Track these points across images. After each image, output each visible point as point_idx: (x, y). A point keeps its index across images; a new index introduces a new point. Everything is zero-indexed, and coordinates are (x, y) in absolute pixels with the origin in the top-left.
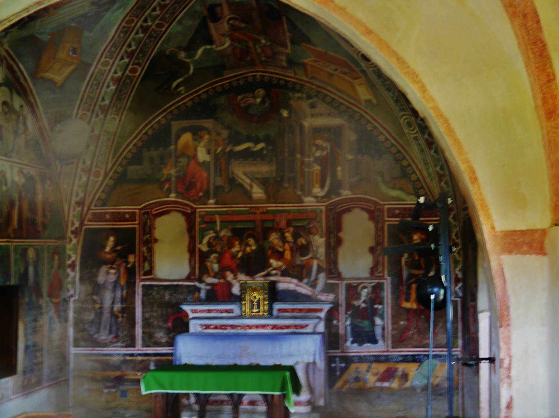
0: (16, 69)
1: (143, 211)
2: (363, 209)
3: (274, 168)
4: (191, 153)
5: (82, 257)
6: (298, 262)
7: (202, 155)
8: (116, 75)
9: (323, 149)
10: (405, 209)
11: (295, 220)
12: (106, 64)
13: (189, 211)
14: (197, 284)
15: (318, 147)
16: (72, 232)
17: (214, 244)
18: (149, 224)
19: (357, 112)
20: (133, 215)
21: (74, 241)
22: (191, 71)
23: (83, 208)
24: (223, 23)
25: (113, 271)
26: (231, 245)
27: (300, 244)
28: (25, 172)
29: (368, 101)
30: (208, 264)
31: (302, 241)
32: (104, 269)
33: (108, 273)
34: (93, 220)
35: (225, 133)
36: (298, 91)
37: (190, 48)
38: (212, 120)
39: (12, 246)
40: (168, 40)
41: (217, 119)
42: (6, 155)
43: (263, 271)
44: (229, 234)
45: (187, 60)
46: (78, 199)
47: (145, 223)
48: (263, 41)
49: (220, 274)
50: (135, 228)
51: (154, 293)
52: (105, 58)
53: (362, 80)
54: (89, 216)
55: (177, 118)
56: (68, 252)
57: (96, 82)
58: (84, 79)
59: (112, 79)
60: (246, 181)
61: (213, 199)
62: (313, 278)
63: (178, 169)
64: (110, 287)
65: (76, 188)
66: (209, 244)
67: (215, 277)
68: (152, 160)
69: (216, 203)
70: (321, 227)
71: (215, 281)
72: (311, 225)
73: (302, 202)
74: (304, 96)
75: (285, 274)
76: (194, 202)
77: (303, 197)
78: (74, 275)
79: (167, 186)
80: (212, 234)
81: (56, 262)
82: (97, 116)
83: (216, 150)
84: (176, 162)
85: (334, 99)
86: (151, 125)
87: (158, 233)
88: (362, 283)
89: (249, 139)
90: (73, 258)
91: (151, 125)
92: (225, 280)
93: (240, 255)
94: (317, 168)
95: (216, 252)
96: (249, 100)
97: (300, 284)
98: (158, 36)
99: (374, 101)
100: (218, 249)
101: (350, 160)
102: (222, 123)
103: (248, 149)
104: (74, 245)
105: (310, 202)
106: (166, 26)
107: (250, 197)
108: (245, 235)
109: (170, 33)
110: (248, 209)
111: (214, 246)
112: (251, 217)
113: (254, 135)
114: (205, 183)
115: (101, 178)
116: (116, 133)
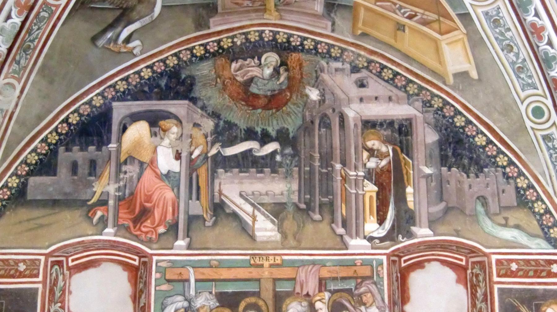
1: (51, 259)
2: (444, 262)
3: (295, 186)
4: (146, 158)
9: (381, 156)
10: (528, 262)
11: (335, 279)
13: (136, 263)
18: (61, 283)
19: (437, 96)
22: (158, 9)
29: (463, 76)
35: (209, 125)
36: (336, 59)
38: (186, 102)
41: (194, 100)
44: (213, 303)
47: (55, 283)
50: (37, 289)
53: (460, 33)
55: (123, 97)
63: (122, 183)
68: (74, 168)
69: (189, 247)
70: (381, 291)
72: (362, 290)
73: (346, 246)
74: (347, 66)
76: (149, 242)
77: (347, 238)
79: (99, 214)
83: (191, 154)
84: (119, 171)
85: (396, 74)
89: (250, 135)
99: (474, 74)
102: (203, 108)
103: (247, 154)
105: (356, 247)
107: (252, 237)
110: (248, 257)
112: (254, 273)
113: (259, 130)
114: (170, 209)
116: (13, 113)
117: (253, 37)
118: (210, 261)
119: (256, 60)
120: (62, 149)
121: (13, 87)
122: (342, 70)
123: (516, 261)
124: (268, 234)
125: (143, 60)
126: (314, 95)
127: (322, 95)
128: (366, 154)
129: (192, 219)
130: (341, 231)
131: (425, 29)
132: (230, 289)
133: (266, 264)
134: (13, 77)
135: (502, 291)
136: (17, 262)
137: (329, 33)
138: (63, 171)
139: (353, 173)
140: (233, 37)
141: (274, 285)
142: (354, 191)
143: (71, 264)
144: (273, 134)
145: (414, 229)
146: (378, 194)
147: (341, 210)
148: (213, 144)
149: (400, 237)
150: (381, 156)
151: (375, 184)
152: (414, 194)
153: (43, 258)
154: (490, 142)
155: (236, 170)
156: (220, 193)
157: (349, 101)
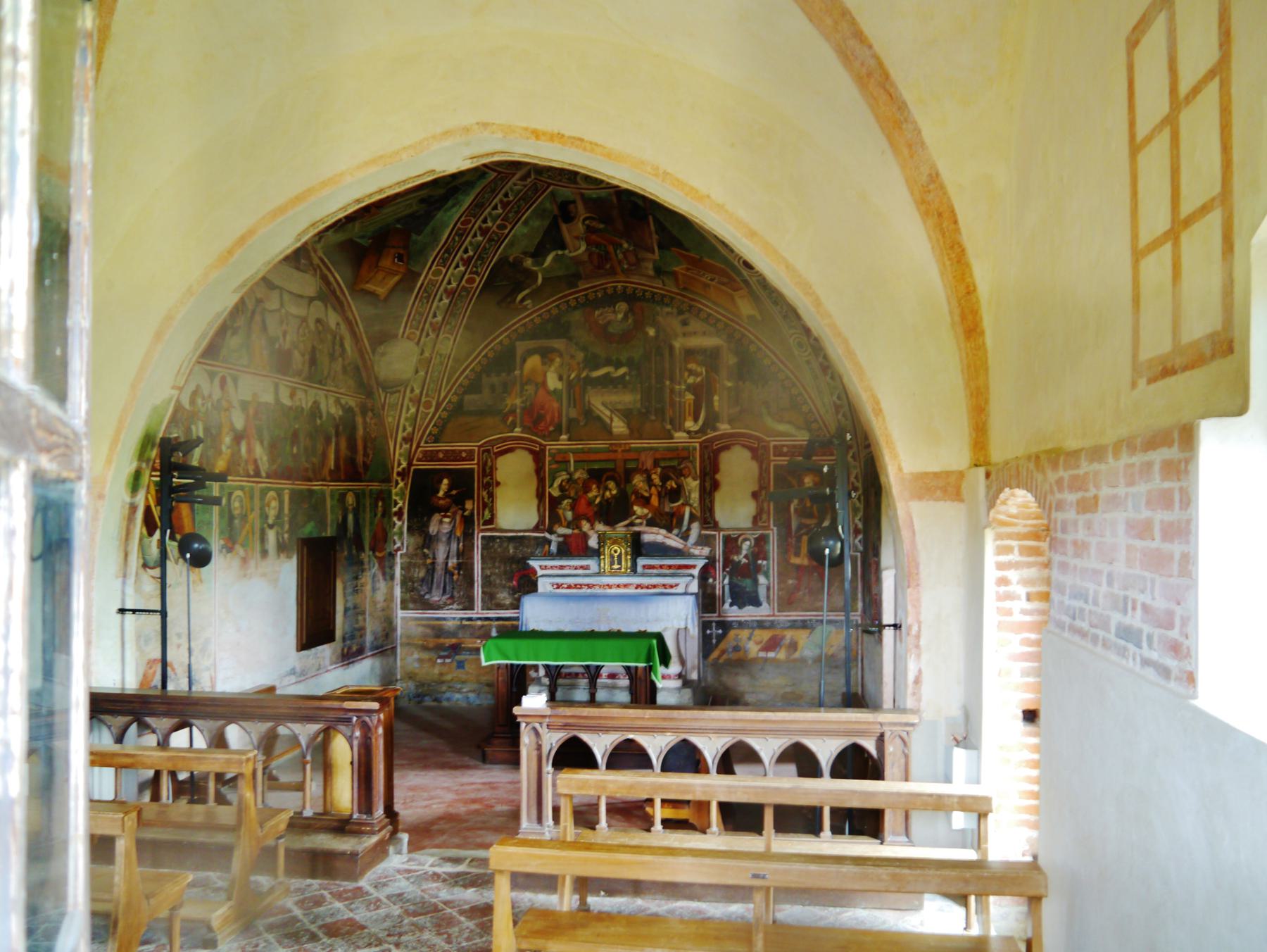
0: (332, 279)
1: (482, 449)
3: (639, 397)
4: (540, 380)
6: (667, 509)
7: (553, 382)
8: (449, 287)
9: (697, 375)
10: (794, 446)
11: (664, 459)
13: (538, 449)
15: (691, 372)
16: (399, 474)
17: (567, 487)
18: (489, 464)
20: (471, 453)
21: (401, 484)
22: (540, 280)
23: (411, 446)
25: (447, 520)
26: (587, 489)
27: (669, 487)
28: (343, 402)
29: (751, 317)
30: (560, 512)
31: (672, 484)
32: (436, 517)
35: (580, 356)
36: (667, 305)
38: (564, 340)
40: (511, 244)
41: (570, 339)
42: (320, 382)
44: (585, 476)
45: (535, 268)
46: (405, 434)
47: (485, 464)
48: (626, 245)
49: (574, 523)
50: (473, 469)
51: (496, 546)
52: (437, 265)
54: (419, 455)
55: (522, 337)
56: (394, 497)
60: (605, 413)
62: (684, 528)
63: (524, 398)
64: (444, 539)
66: (561, 488)
67: (568, 527)
68: (493, 388)
69: (569, 440)
70: (695, 468)
71: (568, 531)
72: (682, 466)
74: (675, 311)
75: (651, 523)
76: (543, 437)
77: (672, 432)
78: (401, 525)
79: (511, 419)
83: (569, 376)
87: (500, 475)
89: (608, 362)
92: (581, 530)
93: (598, 500)
95: (570, 498)
97: (669, 535)
99: (759, 317)
100: (572, 494)
102: (576, 344)
103: (607, 375)
104: (401, 488)
106: (509, 227)
108: (605, 476)
109: (514, 236)
111: (566, 491)
112: (612, 456)
113: (614, 358)
115: (432, 410)
117: (610, 291)
118: (582, 449)
119: (612, 308)
120: (484, 376)
121: (449, 339)
122: (672, 313)
123: (787, 446)
124: (622, 430)
125: (535, 311)
126: (652, 332)
127: (657, 332)
128: (686, 374)
129: (570, 421)
130: (669, 427)
131: (723, 287)
132: (596, 466)
133: (620, 450)
134: (448, 333)
135: (775, 466)
136: (461, 451)
137: (661, 286)
138: (486, 391)
139: (677, 387)
140: (595, 292)
141: (625, 464)
142: (678, 399)
143: (496, 451)
144: (624, 361)
145: (718, 425)
146: (694, 401)
147: (669, 413)
148: (584, 369)
149: (709, 431)
150: (697, 375)
151: (693, 394)
152: (719, 400)
153: (476, 449)
154: (773, 363)
155: (600, 387)
156: (589, 402)
157: (676, 336)
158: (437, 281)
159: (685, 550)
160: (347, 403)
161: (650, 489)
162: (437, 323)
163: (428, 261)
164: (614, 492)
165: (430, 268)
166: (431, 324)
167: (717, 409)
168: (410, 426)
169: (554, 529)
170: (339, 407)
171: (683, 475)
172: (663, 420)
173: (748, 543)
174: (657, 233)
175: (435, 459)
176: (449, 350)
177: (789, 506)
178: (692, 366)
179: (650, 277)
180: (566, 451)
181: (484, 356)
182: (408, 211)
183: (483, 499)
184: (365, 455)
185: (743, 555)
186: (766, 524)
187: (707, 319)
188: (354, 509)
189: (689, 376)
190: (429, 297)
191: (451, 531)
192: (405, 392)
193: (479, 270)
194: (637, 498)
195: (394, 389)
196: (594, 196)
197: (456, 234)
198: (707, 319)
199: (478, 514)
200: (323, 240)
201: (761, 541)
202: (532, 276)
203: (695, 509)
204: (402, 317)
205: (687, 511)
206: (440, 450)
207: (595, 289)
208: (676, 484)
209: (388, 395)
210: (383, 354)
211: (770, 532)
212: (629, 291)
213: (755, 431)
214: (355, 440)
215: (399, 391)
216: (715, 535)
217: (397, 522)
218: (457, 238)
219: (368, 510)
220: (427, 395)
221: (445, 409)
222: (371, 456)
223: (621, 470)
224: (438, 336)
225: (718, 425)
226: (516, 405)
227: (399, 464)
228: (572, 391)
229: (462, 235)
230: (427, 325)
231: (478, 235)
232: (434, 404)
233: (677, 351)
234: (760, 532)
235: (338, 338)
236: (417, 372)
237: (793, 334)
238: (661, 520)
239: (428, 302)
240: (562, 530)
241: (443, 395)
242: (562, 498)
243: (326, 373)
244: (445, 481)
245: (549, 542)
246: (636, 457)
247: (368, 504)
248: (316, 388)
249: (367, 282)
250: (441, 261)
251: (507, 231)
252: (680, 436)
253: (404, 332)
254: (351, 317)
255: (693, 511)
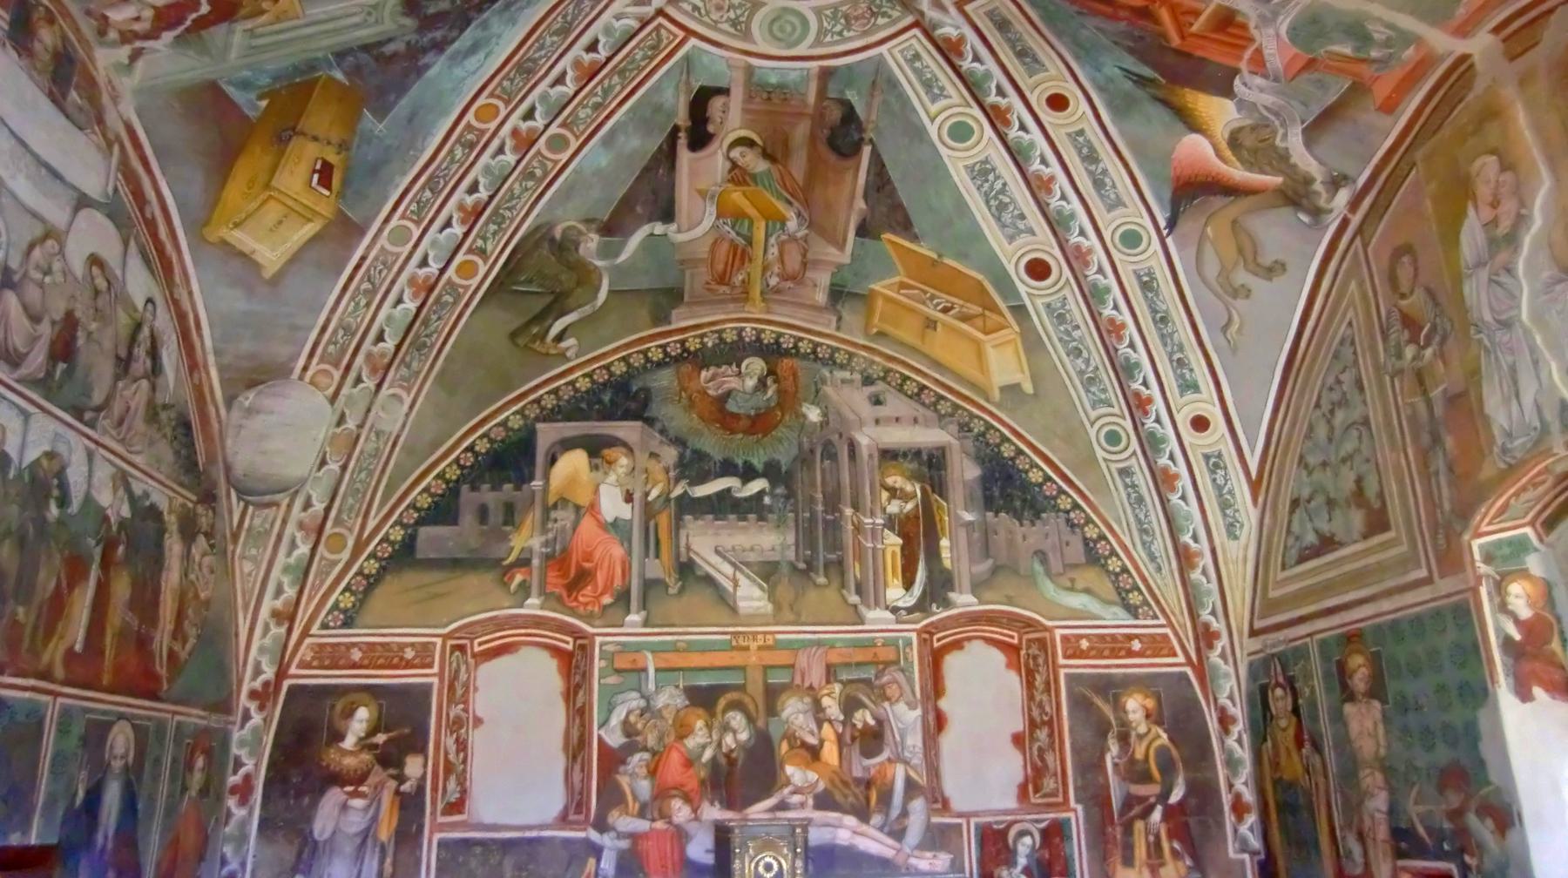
0: (150, 194)
1: (450, 642)
4: (583, 499)
5: (272, 765)
6: (858, 772)
7: (612, 505)
8: (422, 272)
9: (906, 497)
10: (1102, 637)
11: (847, 665)
12: (400, 236)
13: (570, 647)
14: (593, 835)
15: (894, 493)
16: (253, 695)
17: (639, 726)
18: (463, 676)
20: (425, 651)
21: (257, 719)
22: (603, 295)
23: (290, 631)
24: (715, 153)
25: (358, 803)
26: (683, 731)
27: (860, 725)
28: (137, 489)
30: (624, 781)
31: (863, 718)
32: (334, 796)
33: (345, 807)
34: (315, 663)
35: (670, 454)
36: (842, 367)
37: (613, 228)
38: (639, 424)
39: (52, 709)
40: (568, 193)
41: (650, 422)
42: (78, 413)
43: (769, 796)
44: (680, 701)
45: (599, 263)
46: (279, 604)
47: (455, 676)
48: (792, 224)
49: (654, 807)
50: (429, 687)
51: (473, 863)
52: (403, 217)
54: (305, 652)
55: (550, 416)
56: (235, 750)
57: (366, 285)
58: (339, 273)
59: (412, 281)
60: (722, 570)
61: (638, 612)
62: (895, 812)
63: (550, 535)
64: (349, 848)
65: (276, 573)
66: (628, 729)
67: (642, 814)
68: (483, 513)
69: (646, 624)
70: (910, 681)
71: (643, 825)
72: (885, 679)
74: (857, 376)
75: (824, 802)
76: (588, 618)
77: (862, 609)
78: (245, 816)
79: (518, 578)
80: (634, 701)
81: (197, 779)
82: (359, 380)
83: (647, 494)
84: (546, 518)
86: (486, 428)
87: (481, 704)
88: (1016, 822)
89: (727, 468)
90: (249, 766)
91: (486, 428)
92: (670, 823)
93: (708, 754)
94: (893, 541)
95: (645, 749)
96: (724, 382)
97: (864, 828)
98: (546, 174)
99: (1028, 387)
100: (651, 740)
101: (970, 523)
102: (663, 432)
104: (255, 730)
106: (574, 145)
107: (734, 610)
108: (722, 703)
110: (728, 637)
111: (638, 733)
112: (737, 659)
113: (740, 462)
114: (619, 571)
115: (345, 555)
117: (730, 337)
120: (465, 488)
122: (851, 381)
124: (756, 604)
126: (813, 414)
128: (885, 495)
131: (964, 326)
132: (703, 681)
133: (753, 646)
134: (401, 387)
135: (1069, 677)
136: (402, 646)
140: (702, 336)
141: (765, 674)
142: (870, 545)
143: (477, 649)
148: (677, 481)
150: (906, 497)
151: (899, 535)
153: (439, 641)
154: (1048, 479)
155: (711, 517)
156: (688, 548)
157: (861, 423)
158: (398, 255)
159: (900, 860)
160: (146, 495)
161: (820, 727)
162: (383, 355)
163: (386, 199)
164: (743, 736)
165: (387, 220)
166: (369, 356)
167: (947, 563)
168: (293, 584)
169: (610, 820)
170: (121, 492)
171: (888, 699)
172: (843, 585)
173: (1027, 840)
174: (866, 197)
175: (342, 662)
176: (399, 425)
177: (1102, 759)
178: (895, 480)
179: (816, 308)
180: (638, 648)
181: (467, 450)
182: (365, 34)
183: (446, 754)
184: (178, 633)
185: (1019, 868)
186: (1060, 799)
187: (918, 394)
188: (126, 768)
189: (889, 501)
190: (374, 291)
191: (368, 830)
192: (290, 506)
193: (489, 248)
194: (792, 747)
195: (267, 498)
196: (773, 79)
197: (458, 141)
198: (918, 394)
199: (435, 789)
200: (140, 64)
201: (1054, 834)
202: (585, 276)
203: (914, 768)
204: (310, 329)
205: (899, 773)
206: (354, 645)
207: (699, 332)
208: (874, 718)
209: (251, 509)
210: (250, 412)
211: (1071, 815)
212: (767, 338)
213: (1024, 608)
214: (157, 592)
215: (277, 505)
216: (960, 825)
217: (234, 810)
218: (459, 152)
219: (166, 774)
220: (338, 522)
221: (373, 555)
222: (192, 641)
223: (756, 688)
224: (379, 386)
225: (952, 596)
226: (531, 550)
227: (258, 671)
228: (652, 523)
229: (472, 145)
230: (360, 359)
231: (507, 149)
232: (351, 543)
233: (865, 453)
234: (1052, 816)
235: (146, 331)
236: (323, 463)
237: (1099, 418)
238: (846, 796)
239: (368, 305)
240: (626, 822)
241: (371, 524)
242: (630, 748)
243: (98, 397)
244: (363, 713)
245: (597, 851)
246: (791, 662)
247: (167, 761)
248: (57, 418)
249: (236, 225)
250: (414, 207)
251: (564, 157)
252: (877, 618)
253: (305, 369)
254: (186, 305)
255: (912, 774)
